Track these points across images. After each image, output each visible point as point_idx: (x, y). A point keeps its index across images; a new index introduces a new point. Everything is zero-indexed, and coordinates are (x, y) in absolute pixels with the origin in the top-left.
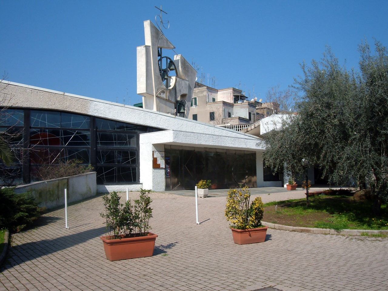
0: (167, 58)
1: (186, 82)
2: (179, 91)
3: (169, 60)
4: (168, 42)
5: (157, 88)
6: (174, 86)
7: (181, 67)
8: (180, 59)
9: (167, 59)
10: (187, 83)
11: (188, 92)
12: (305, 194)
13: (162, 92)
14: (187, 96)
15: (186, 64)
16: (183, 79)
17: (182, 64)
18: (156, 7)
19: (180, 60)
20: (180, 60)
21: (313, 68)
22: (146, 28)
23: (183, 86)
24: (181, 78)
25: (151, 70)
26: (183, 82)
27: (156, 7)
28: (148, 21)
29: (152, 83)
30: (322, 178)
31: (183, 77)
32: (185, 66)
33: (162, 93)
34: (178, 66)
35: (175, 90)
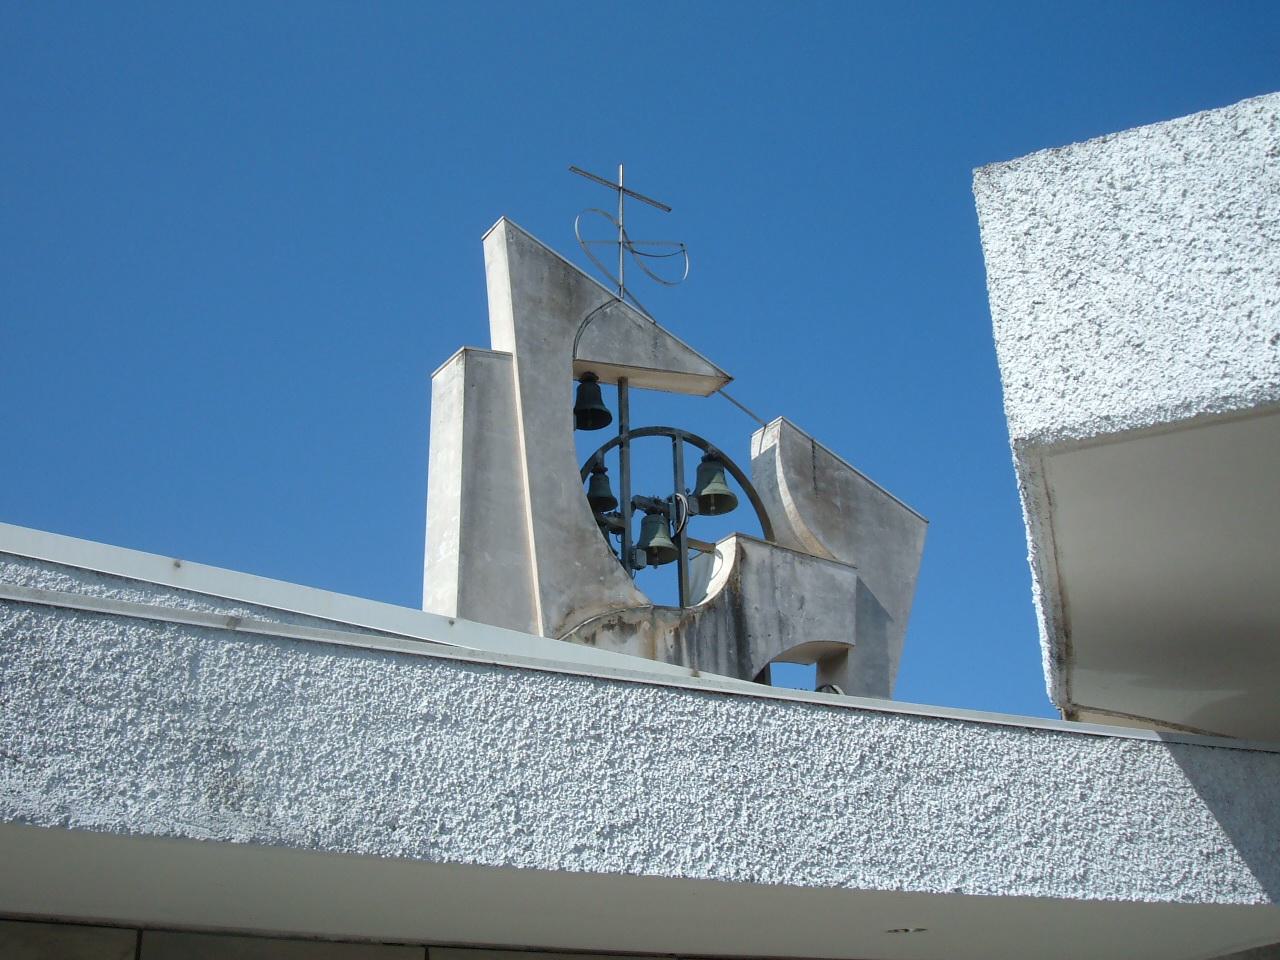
0: (674, 439)
1: (831, 570)
2: (774, 624)
3: (693, 456)
4: (669, 341)
5: (564, 599)
6: (717, 595)
7: (793, 488)
8: (777, 441)
9: (675, 446)
10: (846, 578)
11: (851, 629)
12: (891, 620)
13: (610, 627)
14: (853, 660)
15: (829, 472)
16: (804, 556)
17: (800, 472)
18: (574, 169)
19: (778, 450)
20: (778, 450)
21: (661, 623)
22: (491, 267)
23: (808, 596)
24: (787, 550)
25: (516, 492)
26: (805, 573)
27: (574, 169)
28: (500, 226)
29: (526, 569)
30: (591, 474)
31: (816, 549)
32: (822, 485)
33: (608, 634)
34: (777, 500)
35: (730, 618)
